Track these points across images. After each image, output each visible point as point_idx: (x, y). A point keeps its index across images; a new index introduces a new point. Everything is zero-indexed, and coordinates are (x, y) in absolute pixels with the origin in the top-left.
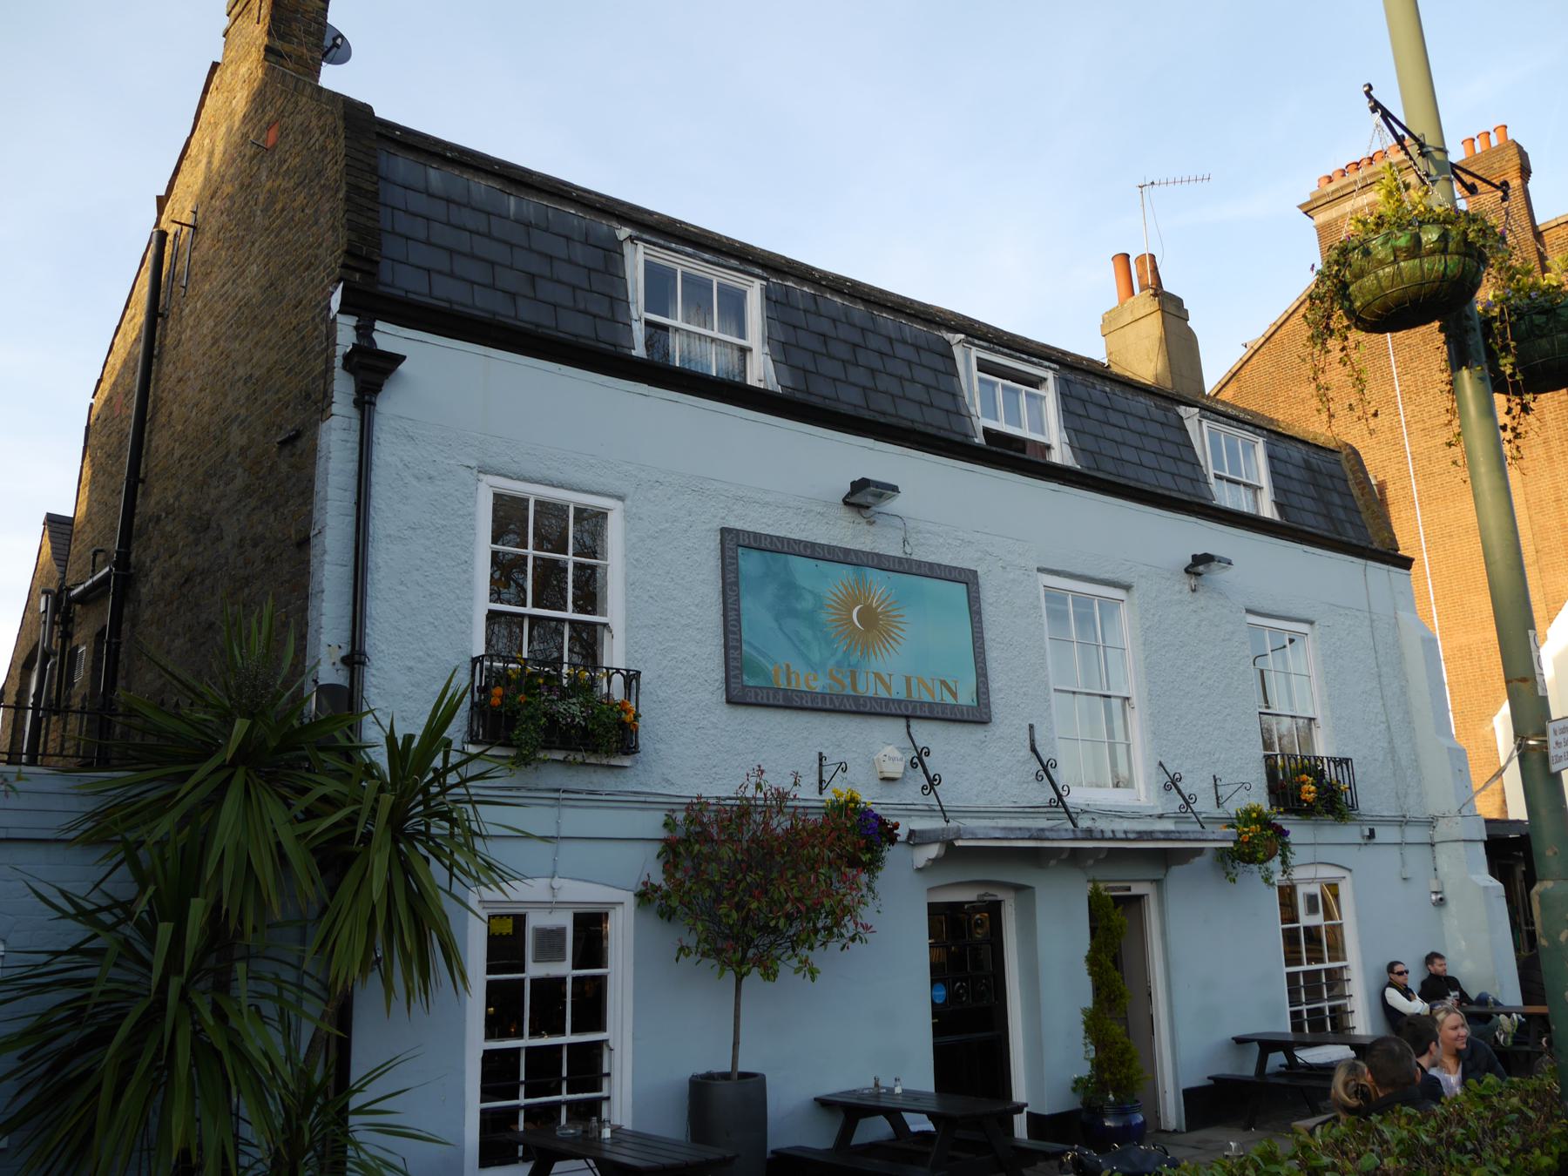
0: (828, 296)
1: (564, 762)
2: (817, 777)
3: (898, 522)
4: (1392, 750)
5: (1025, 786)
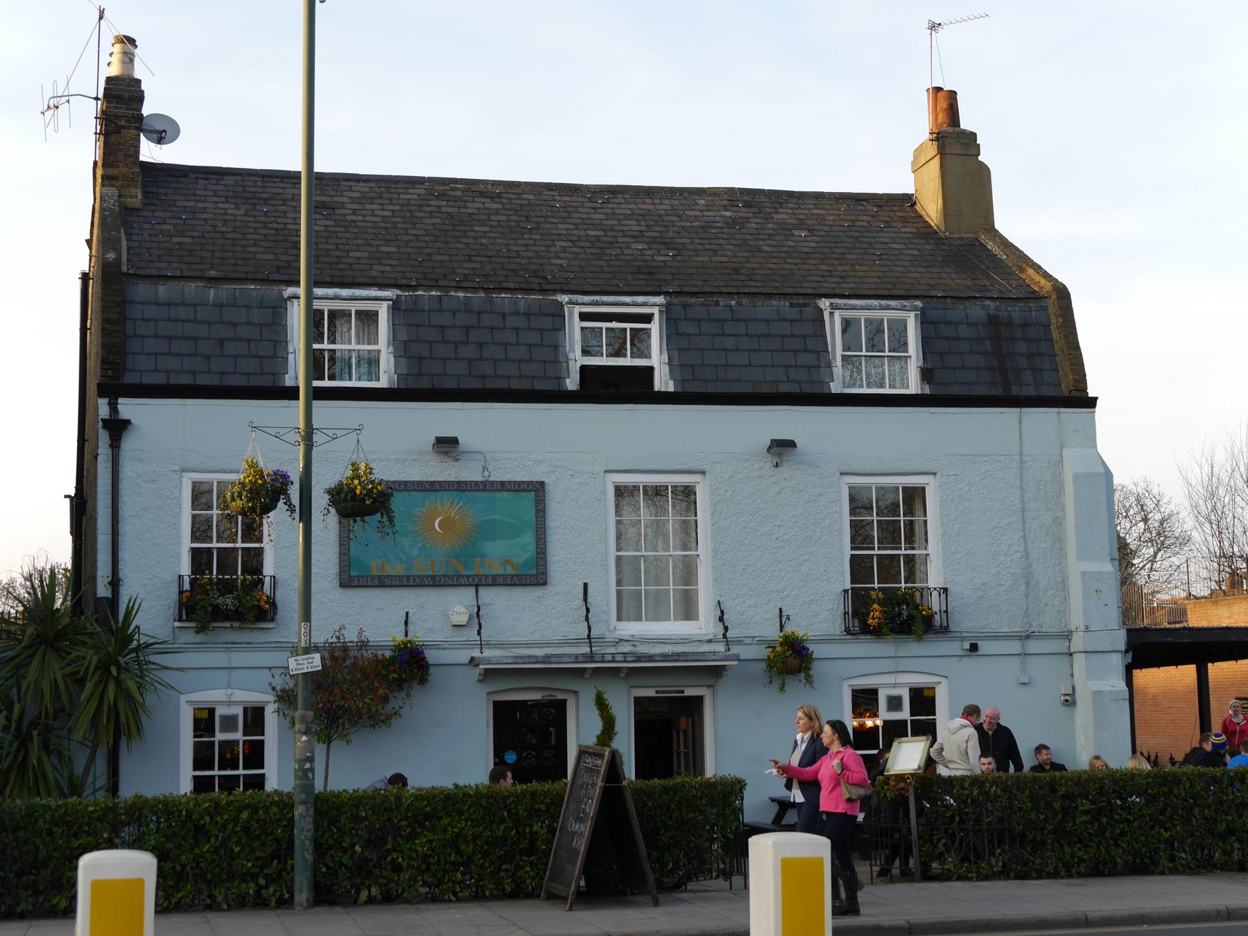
0: (453, 294)
1: (231, 627)
2: (779, 624)
3: (479, 457)
4: (1028, 578)
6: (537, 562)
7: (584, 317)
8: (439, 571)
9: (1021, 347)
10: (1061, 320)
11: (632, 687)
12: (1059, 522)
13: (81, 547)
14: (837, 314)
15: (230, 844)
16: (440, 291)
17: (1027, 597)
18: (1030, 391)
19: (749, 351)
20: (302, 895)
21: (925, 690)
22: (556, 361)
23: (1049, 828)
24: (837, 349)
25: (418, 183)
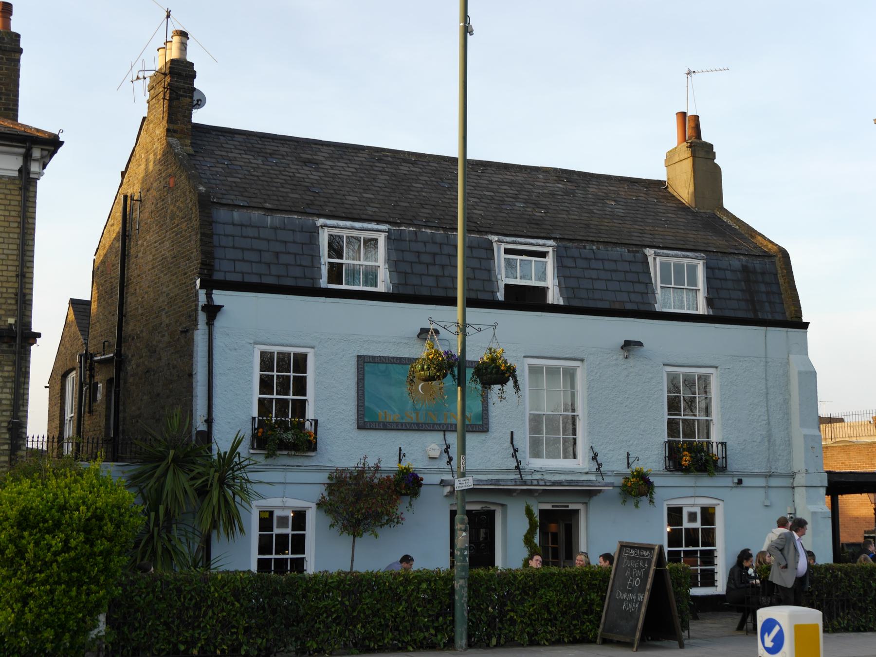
0: (423, 230)
1: (288, 455)
2: (398, 458)
3: (446, 343)
4: (769, 436)
5: (505, 460)
6: (483, 416)
7: (507, 251)
8: (422, 420)
9: (763, 288)
10: (785, 271)
11: (540, 502)
12: (786, 402)
13: (119, 392)
14: (658, 259)
15: (413, 606)
16: (416, 228)
17: (769, 449)
18: (769, 317)
19: (606, 280)
20: (461, 641)
21: (710, 509)
22: (490, 280)
23: (869, 599)
24: (658, 283)
25: (361, 150)
